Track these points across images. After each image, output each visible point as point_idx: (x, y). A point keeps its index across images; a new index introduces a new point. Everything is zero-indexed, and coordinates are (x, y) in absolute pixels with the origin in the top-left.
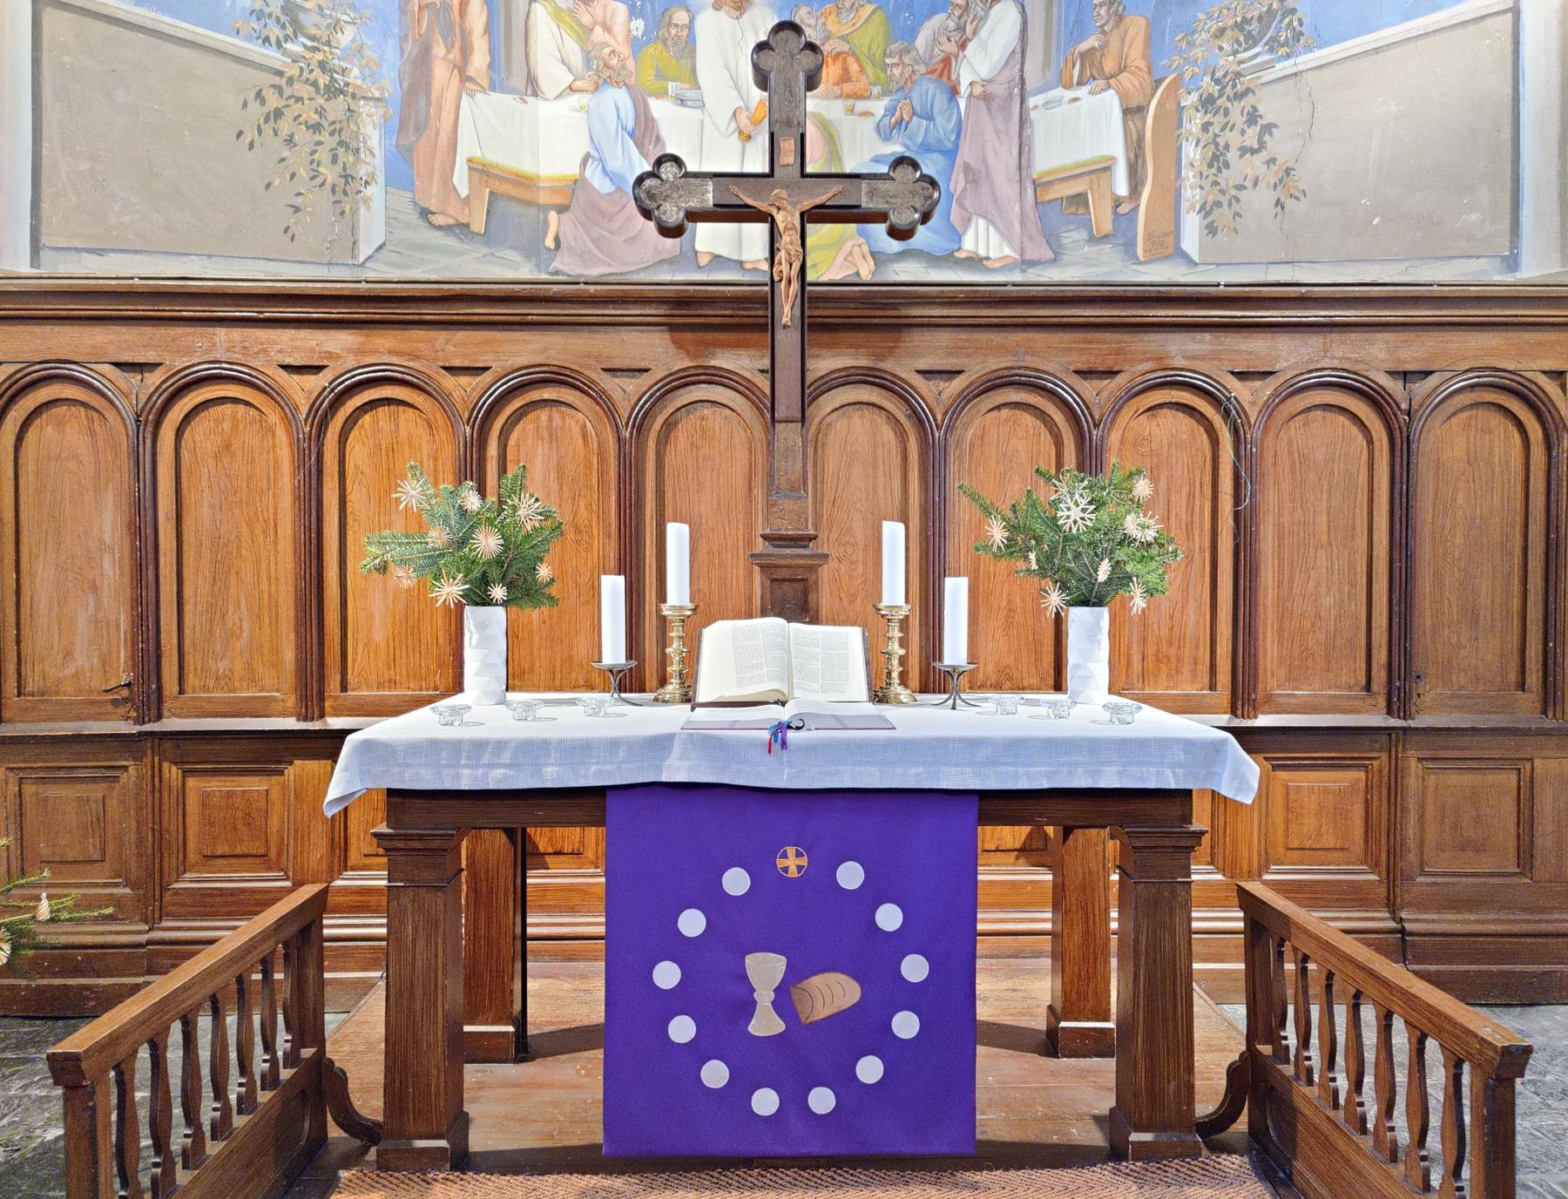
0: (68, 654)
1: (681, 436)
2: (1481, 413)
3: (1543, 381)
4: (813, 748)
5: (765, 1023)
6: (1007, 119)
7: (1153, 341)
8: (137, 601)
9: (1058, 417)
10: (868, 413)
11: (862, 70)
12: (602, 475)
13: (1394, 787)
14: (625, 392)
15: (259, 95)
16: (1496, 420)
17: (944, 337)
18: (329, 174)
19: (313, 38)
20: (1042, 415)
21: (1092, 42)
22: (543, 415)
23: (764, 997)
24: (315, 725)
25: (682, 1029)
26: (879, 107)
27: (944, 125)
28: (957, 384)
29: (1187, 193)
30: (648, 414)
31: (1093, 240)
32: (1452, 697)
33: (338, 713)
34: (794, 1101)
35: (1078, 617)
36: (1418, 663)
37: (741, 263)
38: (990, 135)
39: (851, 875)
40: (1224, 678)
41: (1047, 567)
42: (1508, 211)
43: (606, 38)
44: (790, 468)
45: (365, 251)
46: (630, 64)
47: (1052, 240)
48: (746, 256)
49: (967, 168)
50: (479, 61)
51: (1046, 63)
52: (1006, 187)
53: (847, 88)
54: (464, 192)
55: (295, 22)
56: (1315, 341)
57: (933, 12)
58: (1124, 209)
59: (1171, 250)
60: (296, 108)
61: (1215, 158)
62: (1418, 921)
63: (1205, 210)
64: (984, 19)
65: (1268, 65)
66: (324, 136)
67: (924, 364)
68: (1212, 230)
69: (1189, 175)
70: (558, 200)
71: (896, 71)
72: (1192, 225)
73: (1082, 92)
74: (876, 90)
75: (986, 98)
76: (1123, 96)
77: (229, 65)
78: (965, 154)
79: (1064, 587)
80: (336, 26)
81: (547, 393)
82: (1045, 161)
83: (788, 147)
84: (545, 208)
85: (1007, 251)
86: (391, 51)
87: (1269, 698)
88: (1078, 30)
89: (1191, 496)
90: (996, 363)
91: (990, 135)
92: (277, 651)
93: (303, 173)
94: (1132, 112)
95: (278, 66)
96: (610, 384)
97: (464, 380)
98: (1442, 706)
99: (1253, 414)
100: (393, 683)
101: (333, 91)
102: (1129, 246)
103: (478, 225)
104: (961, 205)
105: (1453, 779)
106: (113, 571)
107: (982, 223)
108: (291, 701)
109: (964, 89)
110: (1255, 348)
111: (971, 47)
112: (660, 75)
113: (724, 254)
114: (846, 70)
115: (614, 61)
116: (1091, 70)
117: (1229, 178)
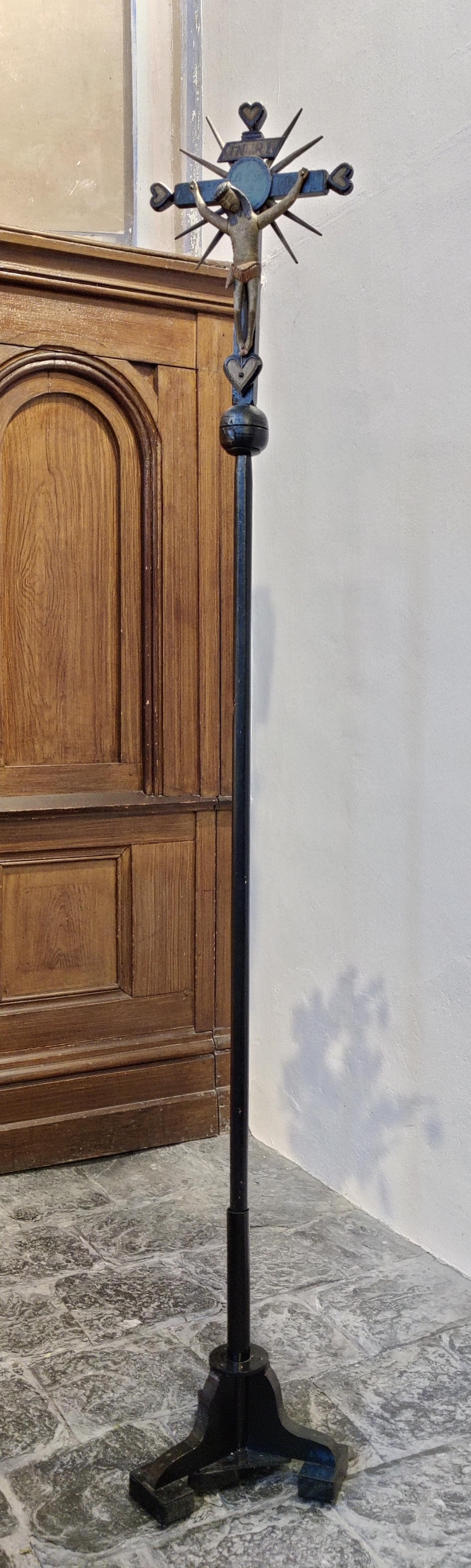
2: (62, 407)
3: (130, 372)
16: (80, 418)
32: (33, 772)
42: (122, 180)
105: (39, 877)
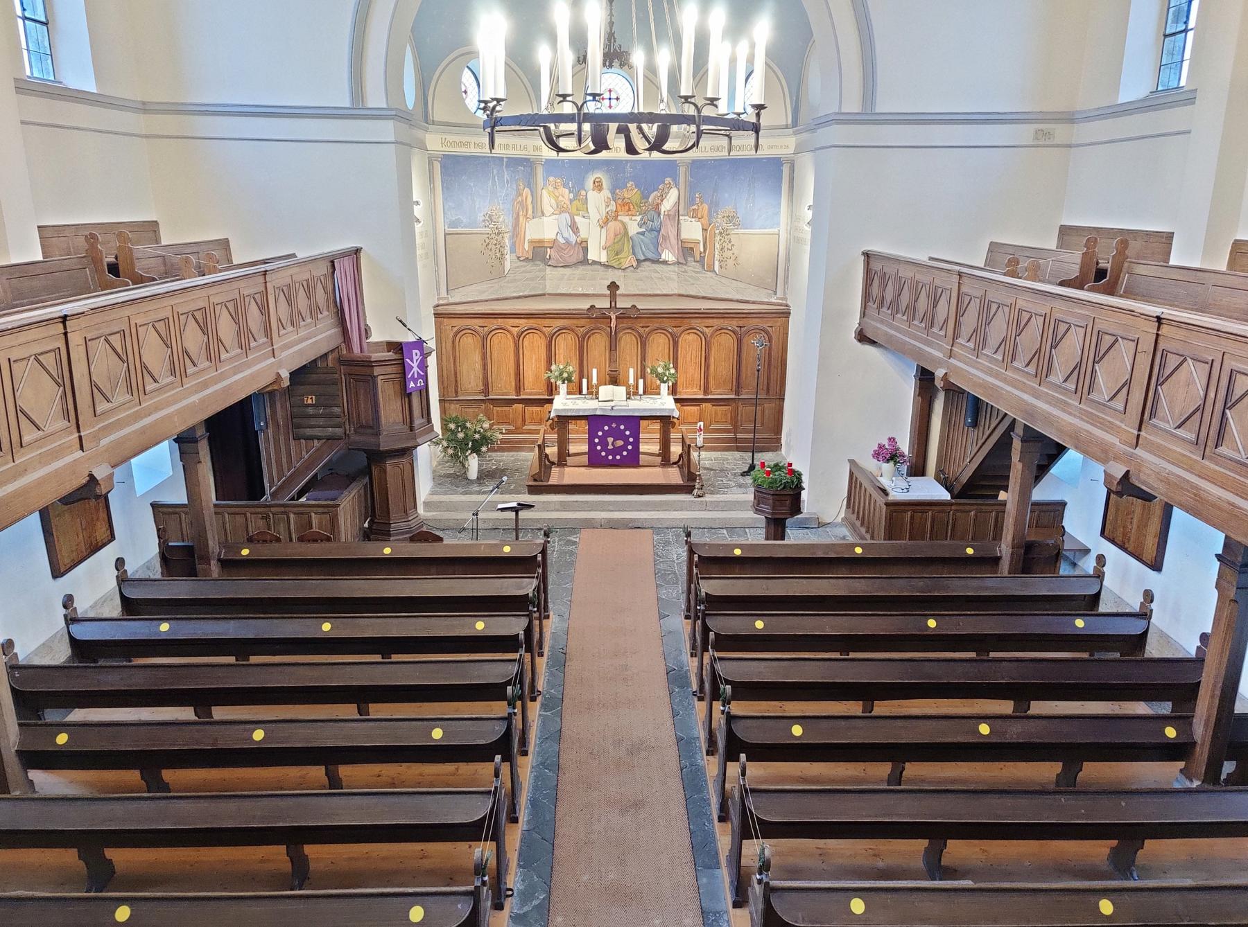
0: (470, 383)
1: (591, 339)
3: (768, 328)
4: (617, 410)
5: (610, 447)
7: (688, 320)
11: (634, 208)
12: (576, 349)
18: (499, 255)
19: (495, 222)
23: (610, 443)
24: (519, 398)
25: (599, 448)
26: (639, 218)
27: (657, 223)
28: (647, 330)
29: (716, 256)
30: (586, 335)
31: (695, 261)
35: (662, 385)
37: (600, 263)
38: (669, 226)
39: (622, 427)
40: (702, 388)
43: (563, 199)
45: (506, 272)
48: (602, 261)
50: (530, 212)
52: (674, 241)
55: (491, 219)
57: (654, 191)
58: (702, 255)
59: (712, 270)
60: (492, 241)
62: (739, 436)
65: (733, 229)
66: (498, 246)
67: (641, 325)
68: (721, 267)
69: (717, 253)
71: (643, 208)
72: (717, 264)
73: (693, 220)
76: (702, 225)
77: (479, 235)
78: (662, 232)
79: (660, 380)
80: (499, 217)
81: (564, 331)
82: (684, 236)
84: (547, 247)
85: (674, 259)
86: (511, 219)
88: (692, 202)
89: (696, 351)
93: (494, 257)
94: (704, 230)
95: (488, 232)
98: (747, 393)
100: (534, 389)
102: (703, 266)
103: (530, 258)
104: (661, 246)
106: (478, 366)
107: (667, 251)
108: (514, 393)
110: (710, 322)
112: (577, 210)
113: (596, 260)
116: (695, 215)
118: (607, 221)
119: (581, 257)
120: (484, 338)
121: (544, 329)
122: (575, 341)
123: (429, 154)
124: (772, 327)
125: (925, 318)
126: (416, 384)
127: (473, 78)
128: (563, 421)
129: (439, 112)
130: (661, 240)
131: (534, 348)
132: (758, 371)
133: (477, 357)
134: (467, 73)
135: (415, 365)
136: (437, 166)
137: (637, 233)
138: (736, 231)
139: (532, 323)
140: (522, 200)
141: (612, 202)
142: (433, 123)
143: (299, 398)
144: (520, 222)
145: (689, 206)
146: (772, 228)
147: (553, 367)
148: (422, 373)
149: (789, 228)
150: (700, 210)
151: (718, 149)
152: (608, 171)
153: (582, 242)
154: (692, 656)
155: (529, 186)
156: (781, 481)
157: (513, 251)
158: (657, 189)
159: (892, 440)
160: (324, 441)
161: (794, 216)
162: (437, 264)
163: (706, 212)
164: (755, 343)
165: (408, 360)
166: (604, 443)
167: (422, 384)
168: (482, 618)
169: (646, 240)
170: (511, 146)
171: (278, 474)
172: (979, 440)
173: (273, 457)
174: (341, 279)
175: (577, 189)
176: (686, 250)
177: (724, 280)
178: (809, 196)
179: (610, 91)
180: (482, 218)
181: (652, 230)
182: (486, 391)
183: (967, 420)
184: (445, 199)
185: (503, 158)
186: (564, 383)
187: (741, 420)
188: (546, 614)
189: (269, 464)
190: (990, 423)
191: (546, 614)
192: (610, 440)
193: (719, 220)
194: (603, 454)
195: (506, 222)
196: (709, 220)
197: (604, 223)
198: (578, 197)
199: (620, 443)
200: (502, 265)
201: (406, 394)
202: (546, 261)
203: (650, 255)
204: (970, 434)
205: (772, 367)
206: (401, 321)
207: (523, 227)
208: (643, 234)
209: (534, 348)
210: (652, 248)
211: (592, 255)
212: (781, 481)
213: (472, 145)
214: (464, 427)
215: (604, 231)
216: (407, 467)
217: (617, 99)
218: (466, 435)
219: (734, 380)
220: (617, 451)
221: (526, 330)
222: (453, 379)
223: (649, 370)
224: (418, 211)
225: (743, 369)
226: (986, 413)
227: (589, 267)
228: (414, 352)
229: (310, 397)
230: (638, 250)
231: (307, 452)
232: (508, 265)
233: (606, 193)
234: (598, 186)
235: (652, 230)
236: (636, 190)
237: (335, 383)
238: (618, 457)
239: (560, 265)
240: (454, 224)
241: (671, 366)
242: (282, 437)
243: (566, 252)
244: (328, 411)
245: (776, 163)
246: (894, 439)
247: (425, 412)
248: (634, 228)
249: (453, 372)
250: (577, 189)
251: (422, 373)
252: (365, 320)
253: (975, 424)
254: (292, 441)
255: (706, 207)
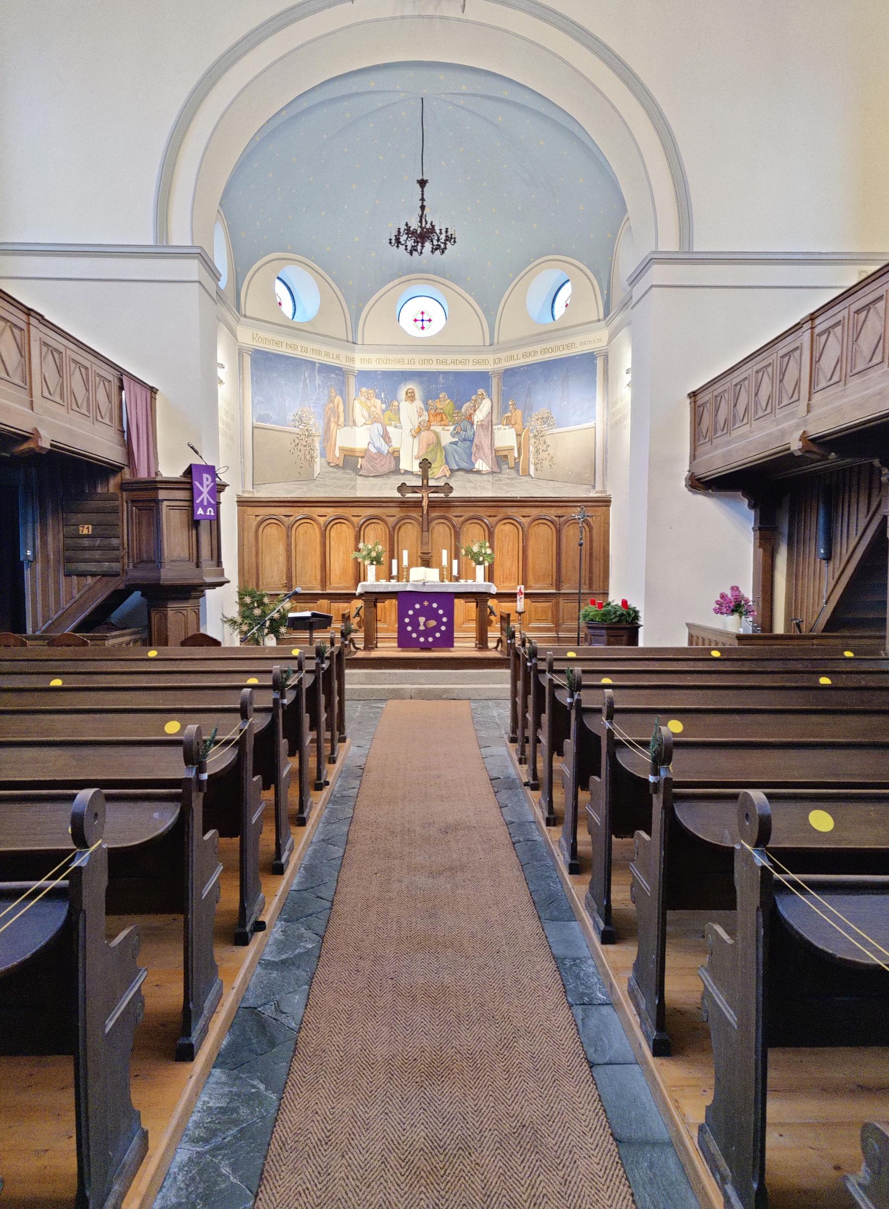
0: (273, 577)
1: (402, 530)
4: (429, 586)
5: (422, 628)
6: (488, 432)
8: (287, 566)
9: (484, 525)
10: (443, 525)
12: (385, 540)
13: (557, 604)
14: (391, 521)
15: (294, 441)
17: (459, 509)
18: (308, 457)
20: (481, 525)
21: (508, 414)
22: (373, 525)
23: (422, 624)
26: (451, 428)
28: (462, 519)
29: (531, 459)
30: (396, 525)
31: (509, 468)
33: (329, 589)
34: (426, 639)
35: (478, 567)
36: (563, 579)
38: (483, 436)
39: (435, 605)
41: (472, 558)
43: (375, 409)
44: (425, 540)
45: (316, 475)
46: (382, 416)
47: (499, 466)
49: (476, 445)
50: (342, 419)
51: (498, 418)
52: (487, 450)
53: (442, 423)
54: (338, 456)
55: (301, 420)
56: (539, 509)
58: (517, 461)
60: (301, 442)
61: (537, 451)
62: (561, 635)
63: (535, 464)
64: (481, 403)
65: (547, 430)
67: (455, 514)
68: (536, 469)
70: (361, 455)
72: (532, 467)
74: (451, 423)
75: (482, 425)
76: (516, 431)
77: (288, 434)
78: (476, 441)
81: (374, 521)
83: (425, 481)
84: (358, 457)
85: (488, 469)
86: (321, 422)
87: (530, 586)
88: (505, 409)
90: (471, 514)
91: (483, 436)
92: (316, 576)
94: (518, 435)
96: (387, 519)
97: (356, 518)
98: (570, 588)
99: (526, 526)
100: (341, 583)
101: (309, 436)
102: (518, 471)
103: (341, 465)
106: (282, 559)
107: (481, 461)
108: (319, 587)
109: (475, 423)
110: (527, 511)
111: (477, 411)
112: (390, 420)
113: (408, 469)
114: (442, 418)
115: (377, 416)
116: (509, 422)
117: (540, 457)
118: (419, 431)
119: (393, 466)
120: (290, 528)
121: (353, 519)
122: (385, 532)
123: (239, 346)
124: (592, 516)
125: (770, 403)
126: (205, 511)
127: (288, 293)
128: (374, 598)
129: (251, 306)
130: (474, 449)
131: (341, 536)
132: (581, 545)
133: (281, 549)
134: (279, 285)
135: (205, 490)
136: (247, 360)
137: (450, 443)
138: (551, 431)
139: (340, 511)
140: (334, 407)
141: (425, 413)
142: (245, 316)
143: (75, 527)
144: (332, 428)
145: (502, 413)
146: (587, 422)
147: (361, 545)
148: (213, 502)
149: (605, 419)
150: (514, 417)
151: (530, 354)
152: (421, 383)
153: (394, 452)
154: (520, 763)
155: (341, 393)
156: (615, 613)
157: (323, 455)
158: (470, 400)
159: (735, 589)
160: (98, 577)
161: (609, 403)
162: (243, 455)
163: (520, 417)
164: (571, 535)
165: (197, 483)
166: (415, 624)
167: (212, 514)
168: (255, 675)
169: (459, 450)
170: (323, 353)
171: (43, 617)
172: (836, 570)
173: (39, 598)
174: (130, 402)
175: (390, 399)
176: (500, 459)
177: (541, 483)
178: (624, 393)
179: (423, 313)
180: (292, 418)
181: (465, 440)
182: (289, 585)
183: (819, 551)
184: (254, 393)
185: (315, 363)
186: (372, 564)
187: (563, 617)
188: (342, 736)
189: (34, 594)
190: (847, 546)
191: (342, 736)
192: (422, 620)
193: (534, 424)
194: (414, 635)
195: (316, 425)
196: (523, 425)
197: (417, 433)
198: (391, 408)
199: (432, 623)
200: (312, 467)
201: (195, 524)
202: (356, 471)
203: (464, 465)
204: (825, 569)
205: (594, 559)
206: (192, 448)
207: (334, 433)
208: (455, 443)
209: (341, 536)
210: (466, 458)
211: (404, 465)
212: (615, 613)
213: (284, 345)
214: (261, 604)
215: (416, 440)
216: (192, 616)
217: (430, 320)
218: (263, 612)
219: (554, 574)
220: (429, 632)
221: (332, 520)
222: (254, 571)
223: (463, 552)
224: (222, 373)
225: (563, 562)
226: (841, 539)
227: (401, 477)
228: (205, 476)
229: (86, 526)
230: (451, 460)
231: (78, 592)
232: (317, 469)
233: (418, 403)
234: (411, 397)
235: (465, 440)
236: (449, 401)
237: (115, 511)
238: (430, 639)
239: (372, 475)
240: (261, 418)
241: (487, 544)
242: (51, 571)
243: (377, 462)
244: (106, 542)
245: (589, 359)
246: (737, 588)
247: (215, 554)
248: (447, 438)
249: (254, 564)
250: (390, 399)
251: (213, 502)
252: (157, 464)
253: (828, 557)
254: (62, 578)
255: (519, 412)
